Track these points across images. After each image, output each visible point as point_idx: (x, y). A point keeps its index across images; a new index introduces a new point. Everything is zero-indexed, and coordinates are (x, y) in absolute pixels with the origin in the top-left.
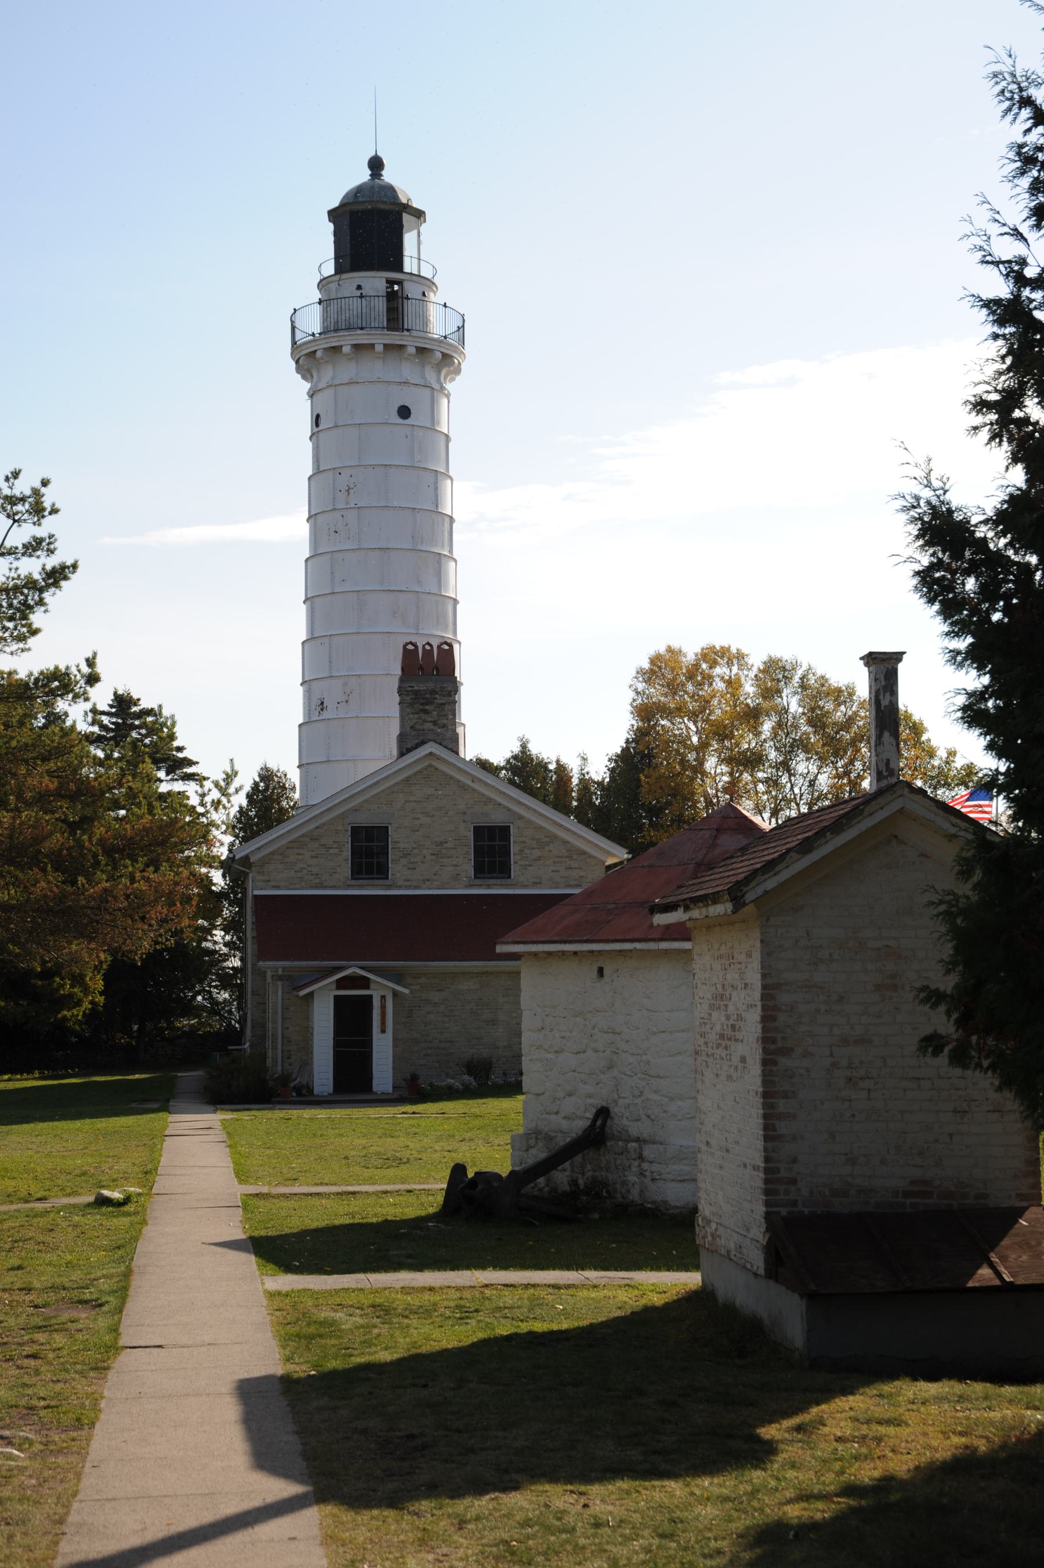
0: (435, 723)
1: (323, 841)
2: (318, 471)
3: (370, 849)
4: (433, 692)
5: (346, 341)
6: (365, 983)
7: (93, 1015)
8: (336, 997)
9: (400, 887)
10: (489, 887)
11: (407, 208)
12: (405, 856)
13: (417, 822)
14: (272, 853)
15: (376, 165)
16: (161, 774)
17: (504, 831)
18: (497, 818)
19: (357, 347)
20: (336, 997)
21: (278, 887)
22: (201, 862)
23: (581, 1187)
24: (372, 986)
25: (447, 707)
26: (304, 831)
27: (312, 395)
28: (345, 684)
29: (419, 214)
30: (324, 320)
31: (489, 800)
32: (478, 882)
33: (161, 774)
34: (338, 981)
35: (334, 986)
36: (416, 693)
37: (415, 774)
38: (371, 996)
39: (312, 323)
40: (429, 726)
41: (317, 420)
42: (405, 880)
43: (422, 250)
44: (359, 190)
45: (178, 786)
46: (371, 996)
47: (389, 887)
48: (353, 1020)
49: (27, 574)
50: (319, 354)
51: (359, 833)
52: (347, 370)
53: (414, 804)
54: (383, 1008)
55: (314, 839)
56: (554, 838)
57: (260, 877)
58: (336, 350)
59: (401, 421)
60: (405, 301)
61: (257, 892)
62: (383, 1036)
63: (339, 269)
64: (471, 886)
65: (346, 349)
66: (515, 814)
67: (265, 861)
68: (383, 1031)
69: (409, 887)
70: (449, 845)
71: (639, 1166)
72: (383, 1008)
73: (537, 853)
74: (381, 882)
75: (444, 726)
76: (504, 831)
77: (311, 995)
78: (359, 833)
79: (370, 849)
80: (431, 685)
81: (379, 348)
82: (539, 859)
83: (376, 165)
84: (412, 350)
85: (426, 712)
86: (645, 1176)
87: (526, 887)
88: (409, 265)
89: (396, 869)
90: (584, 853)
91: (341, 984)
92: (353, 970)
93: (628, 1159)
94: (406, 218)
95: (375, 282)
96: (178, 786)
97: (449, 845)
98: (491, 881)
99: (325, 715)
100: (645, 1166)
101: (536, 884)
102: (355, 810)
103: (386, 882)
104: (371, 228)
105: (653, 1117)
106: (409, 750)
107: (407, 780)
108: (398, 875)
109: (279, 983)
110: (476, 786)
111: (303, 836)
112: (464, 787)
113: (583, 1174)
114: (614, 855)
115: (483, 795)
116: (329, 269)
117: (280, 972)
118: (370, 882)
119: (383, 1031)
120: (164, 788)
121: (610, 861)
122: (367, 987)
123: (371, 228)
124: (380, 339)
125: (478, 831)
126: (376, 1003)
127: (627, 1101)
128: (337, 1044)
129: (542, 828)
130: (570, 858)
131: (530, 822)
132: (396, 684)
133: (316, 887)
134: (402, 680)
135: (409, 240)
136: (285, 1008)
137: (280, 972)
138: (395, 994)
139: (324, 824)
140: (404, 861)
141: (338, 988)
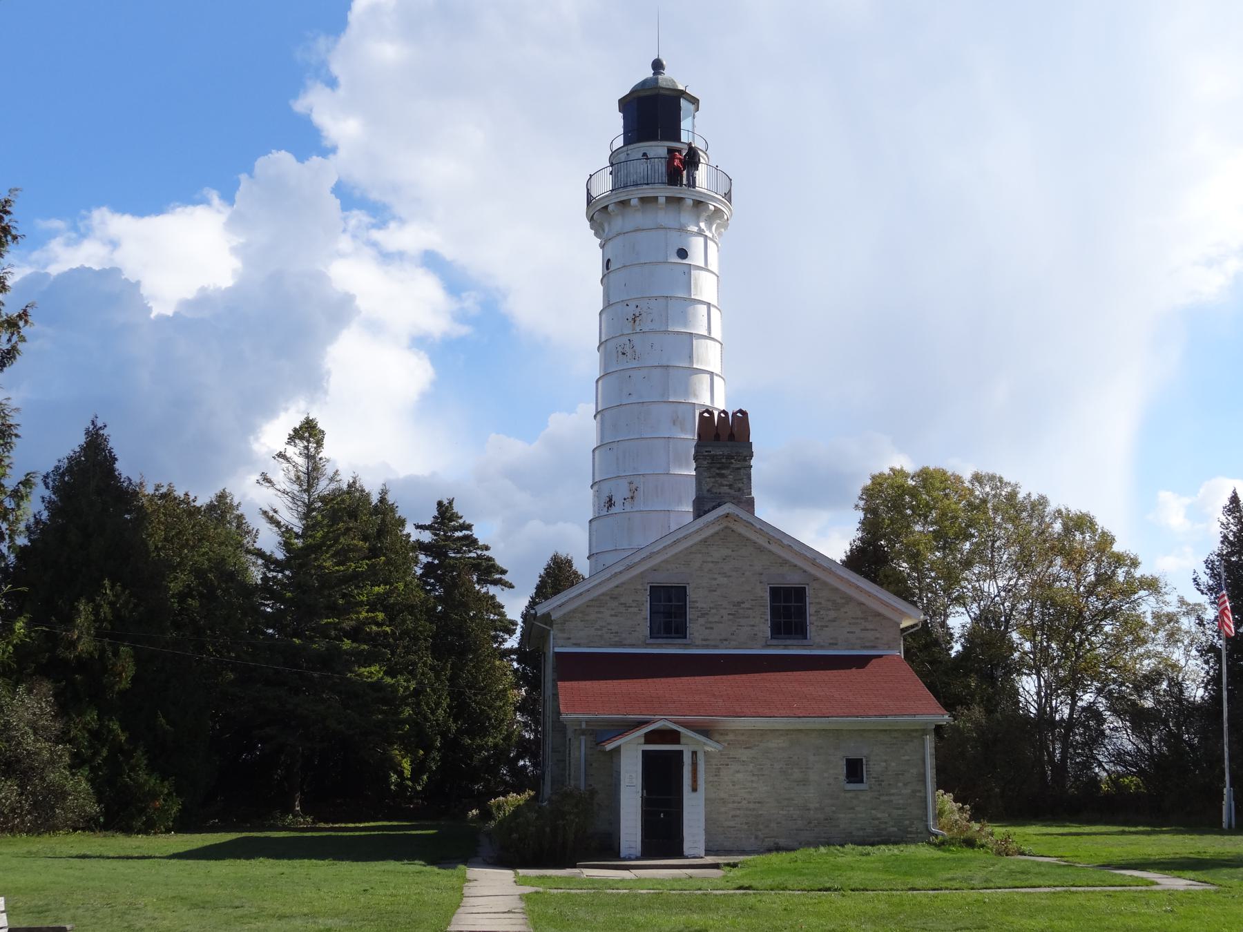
0: (730, 486)
1: (622, 600)
2: (608, 305)
3: (669, 608)
4: (730, 457)
5: (634, 195)
6: (673, 737)
7: (135, 679)
8: (643, 751)
9: (697, 647)
10: (786, 647)
11: (682, 93)
12: (703, 615)
13: (714, 582)
14: (574, 611)
15: (658, 66)
17: (799, 593)
18: (793, 580)
19: (644, 200)
20: (643, 751)
21: (578, 645)
24: (682, 740)
25: (742, 471)
26: (604, 589)
27: (602, 246)
28: (631, 483)
29: (694, 101)
30: (614, 183)
31: (785, 562)
32: (775, 642)
34: (646, 734)
35: (643, 740)
36: (712, 457)
37: (712, 536)
38: (681, 752)
39: (604, 185)
40: (726, 489)
41: (607, 264)
42: (701, 639)
43: (693, 129)
46: (681, 752)
47: (686, 646)
48: (663, 777)
49: (403, 516)
50: (610, 208)
51: (777, 593)
52: (637, 218)
53: (711, 565)
55: (614, 598)
56: (849, 599)
57: (560, 635)
58: (624, 203)
59: (680, 261)
60: (558, 645)
61: (557, 650)
62: (694, 794)
63: (628, 141)
64: (767, 646)
65: (634, 202)
66: (811, 575)
67: (566, 619)
68: (694, 789)
69: (707, 647)
70: (746, 605)
73: (833, 614)
74: (679, 641)
75: (739, 490)
76: (799, 593)
77: (617, 750)
79: (669, 608)
80: (726, 451)
81: (662, 200)
82: (834, 620)
83: (658, 66)
84: (690, 202)
85: (723, 476)
87: (822, 647)
88: (684, 137)
89: (695, 628)
90: (879, 615)
91: (650, 738)
95: (658, 149)
97: (746, 605)
98: (789, 642)
99: (613, 510)
101: (833, 645)
102: (654, 570)
103: (684, 641)
104: (653, 112)
106: (706, 512)
107: (705, 541)
108: (696, 634)
109: (583, 738)
110: (774, 548)
111: (603, 594)
112: (761, 549)
114: (910, 617)
115: (780, 557)
116: (619, 142)
117: (584, 726)
118: (670, 641)
119: (694, 789)
121: (904, 624)
122: (677, 742)
123: (653, 112)
124: (663, 192)
125: (775, 592)
126: (687, 759)
129: (837, 589)
130: (865, 619)
131: (825, 584)
133: (615, 646)
134: (698, 446)
135: (685, 124)
136: (588, 764)
137: (584, 726)
139: (623, 583)
140: (702, 621)
141: (647, 742)
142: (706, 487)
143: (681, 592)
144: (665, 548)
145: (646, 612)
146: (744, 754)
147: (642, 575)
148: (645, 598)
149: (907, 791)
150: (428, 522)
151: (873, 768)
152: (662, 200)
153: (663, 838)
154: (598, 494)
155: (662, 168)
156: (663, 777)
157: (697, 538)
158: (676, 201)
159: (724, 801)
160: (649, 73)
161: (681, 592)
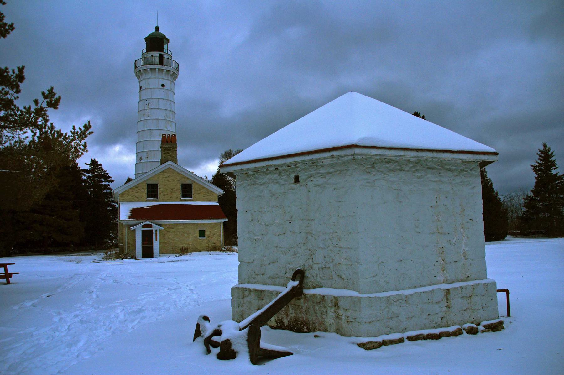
5: (149, 67)
6: (150, 226)
15: (157, 28)
16: (103, 180)
17: (190, 186)
18: (188, 182)
22: (113, 202)
23: (286, 324)
31: (186, 177)
33: (103, 180)
36: (165, 148)
43: (170, 48)
44: (153, 33)
45: (107, 183)
48: (147, 237)
51: (149, 186)
54: (156, 234)
56: (204, 188)
63: (147, 51)
68: (156, 240)
71: (335, 312)
72: (156, 234)
73: (199, 192)
76: (190, 186)
78: (149, 186)
80: (170, 146)
81: (157, 70)
83: (157, 28)
86: (341, 319)
88: (165, 51)
89: (158, 55)
91: (144, 226)
92: (148, 223)
93: (325, 307)
94: (165, 41)
95: (156, 54)
96: (107, 183)
100: (341, 312)
102: (148, 180)
104: (156, 42)
105: (344, 277)
110: (182, 173)
112: (179, 174)
113: (287, 316)
116: (145, 51)
119: (156, 240)
120: (103, 183)
122: (151, 227)
123: (156, 42)
124: (158, 67)
127: (320, 266)
128: (143, 244)
132: (160, 145)
135: (165, 47)
136: (128, 234)
138: (160, 230)
142: (163, 156)
143: (156, 186)
144: (344, 156)
145: (146, 191)
146: (172, 230)
147: (145, 181)
148: (146, 188)
149: (216, 239)
150: (89, 163)
151: (207, 233)
152: (157, 70)
153: (148, 253)
154: (137, 157)
155: (157, 60)
156: (147, 237)
157: (161, 171)
158: (161, 70)
159: (166, 243)
160: (154, 30)
161: (156, 186)
